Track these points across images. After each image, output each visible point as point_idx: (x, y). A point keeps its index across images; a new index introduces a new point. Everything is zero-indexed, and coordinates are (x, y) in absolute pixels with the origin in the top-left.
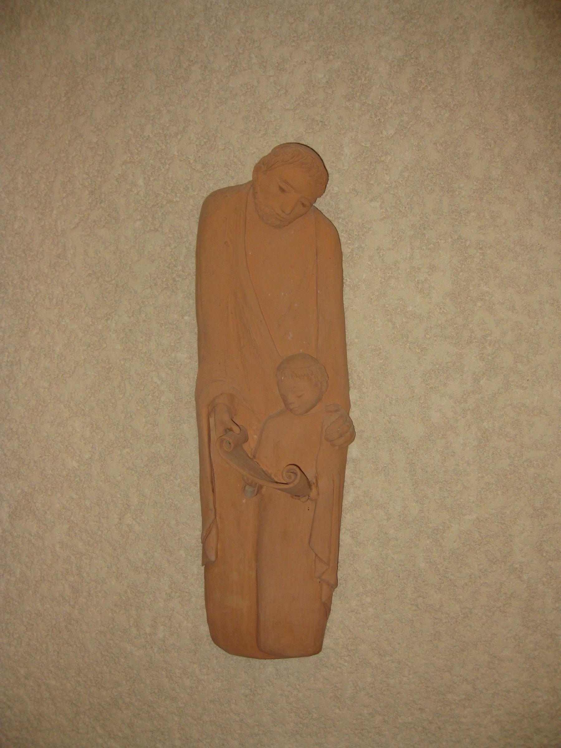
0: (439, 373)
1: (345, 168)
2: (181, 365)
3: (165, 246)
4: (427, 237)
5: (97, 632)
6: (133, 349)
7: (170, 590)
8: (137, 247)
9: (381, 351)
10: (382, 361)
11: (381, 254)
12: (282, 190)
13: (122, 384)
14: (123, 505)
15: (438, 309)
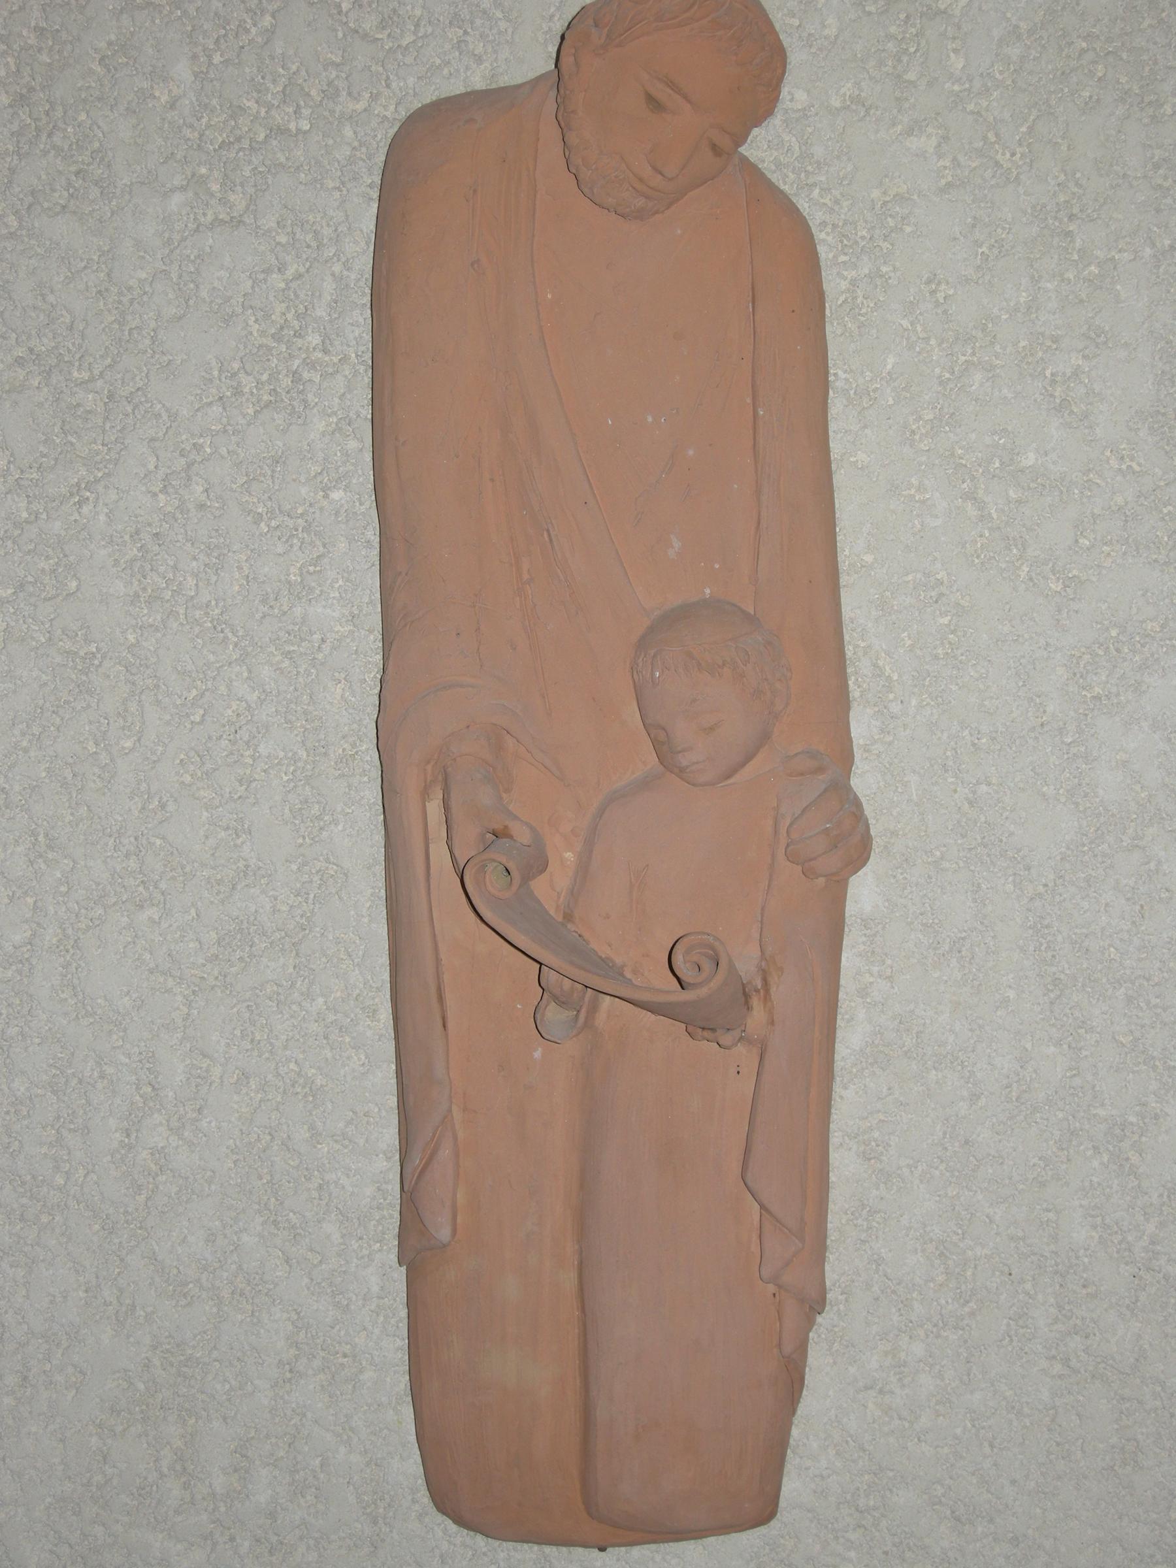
0: (1118, 650)
1: (826, 32)
2: (323, 641)
3: (268, 271)
4: (1078, 243)
5: (49, 1500)
6: (168, 595)
7: (293, 1351)
8: (174, 276)
9: (943, 589)
10: (946, 620)
11: (940, 296)
12: (654, 104)
13: (133, 707)
14: (138, 1088)
15: (1114, 463)
